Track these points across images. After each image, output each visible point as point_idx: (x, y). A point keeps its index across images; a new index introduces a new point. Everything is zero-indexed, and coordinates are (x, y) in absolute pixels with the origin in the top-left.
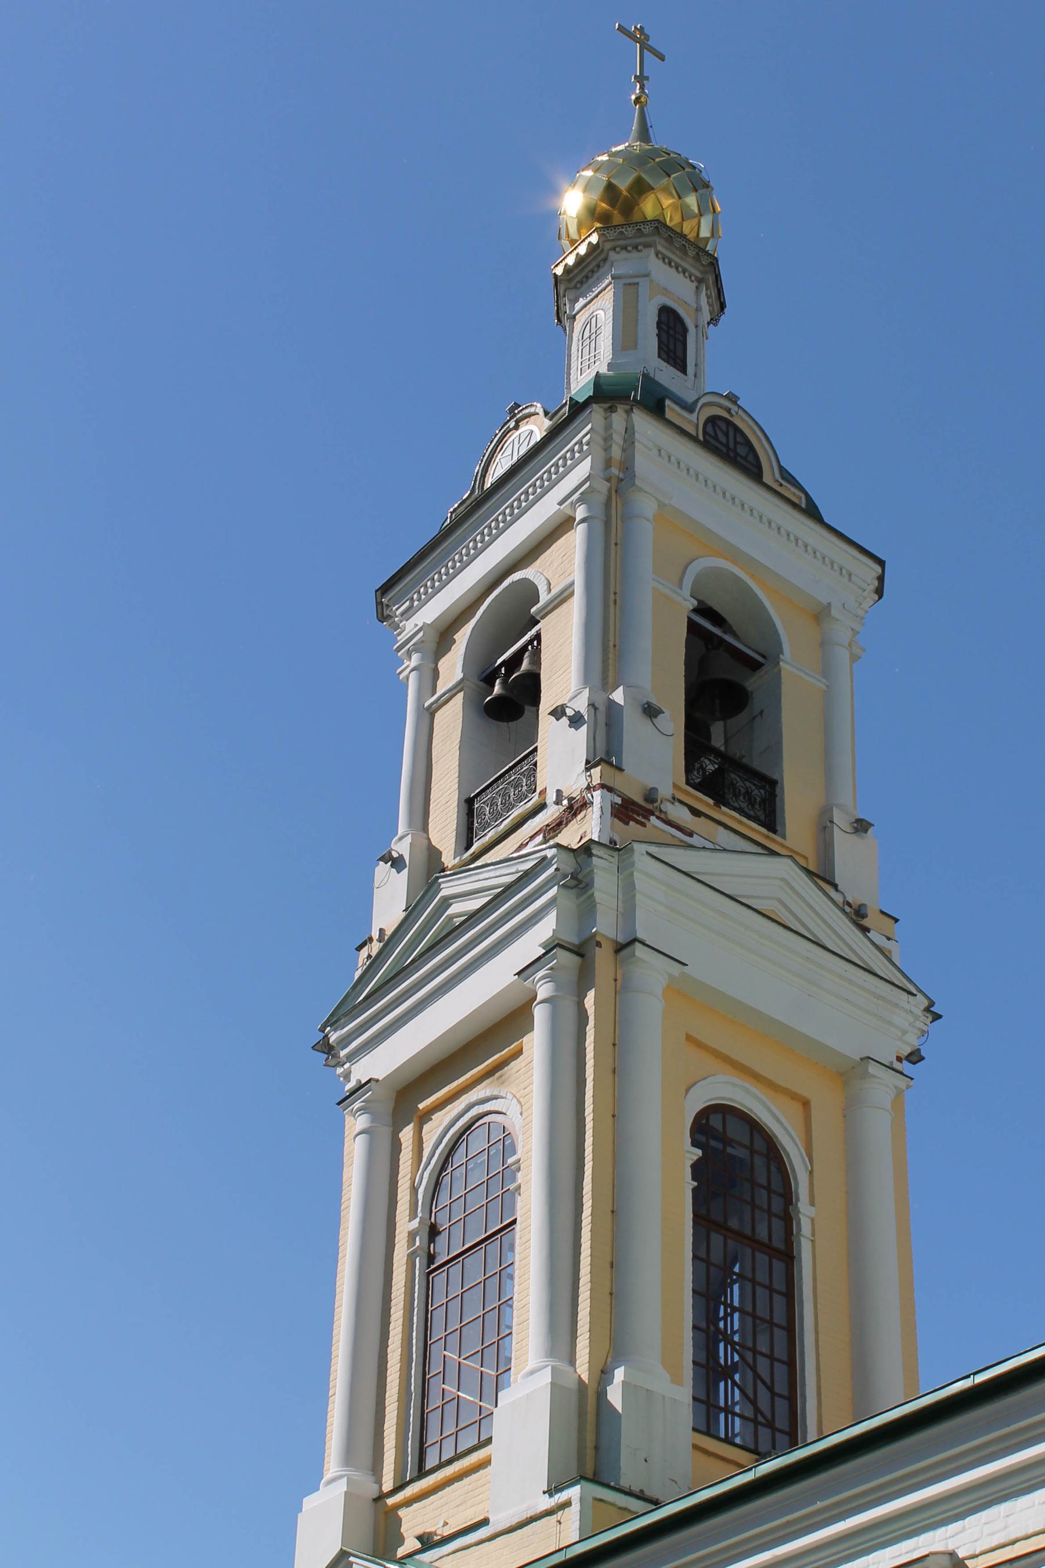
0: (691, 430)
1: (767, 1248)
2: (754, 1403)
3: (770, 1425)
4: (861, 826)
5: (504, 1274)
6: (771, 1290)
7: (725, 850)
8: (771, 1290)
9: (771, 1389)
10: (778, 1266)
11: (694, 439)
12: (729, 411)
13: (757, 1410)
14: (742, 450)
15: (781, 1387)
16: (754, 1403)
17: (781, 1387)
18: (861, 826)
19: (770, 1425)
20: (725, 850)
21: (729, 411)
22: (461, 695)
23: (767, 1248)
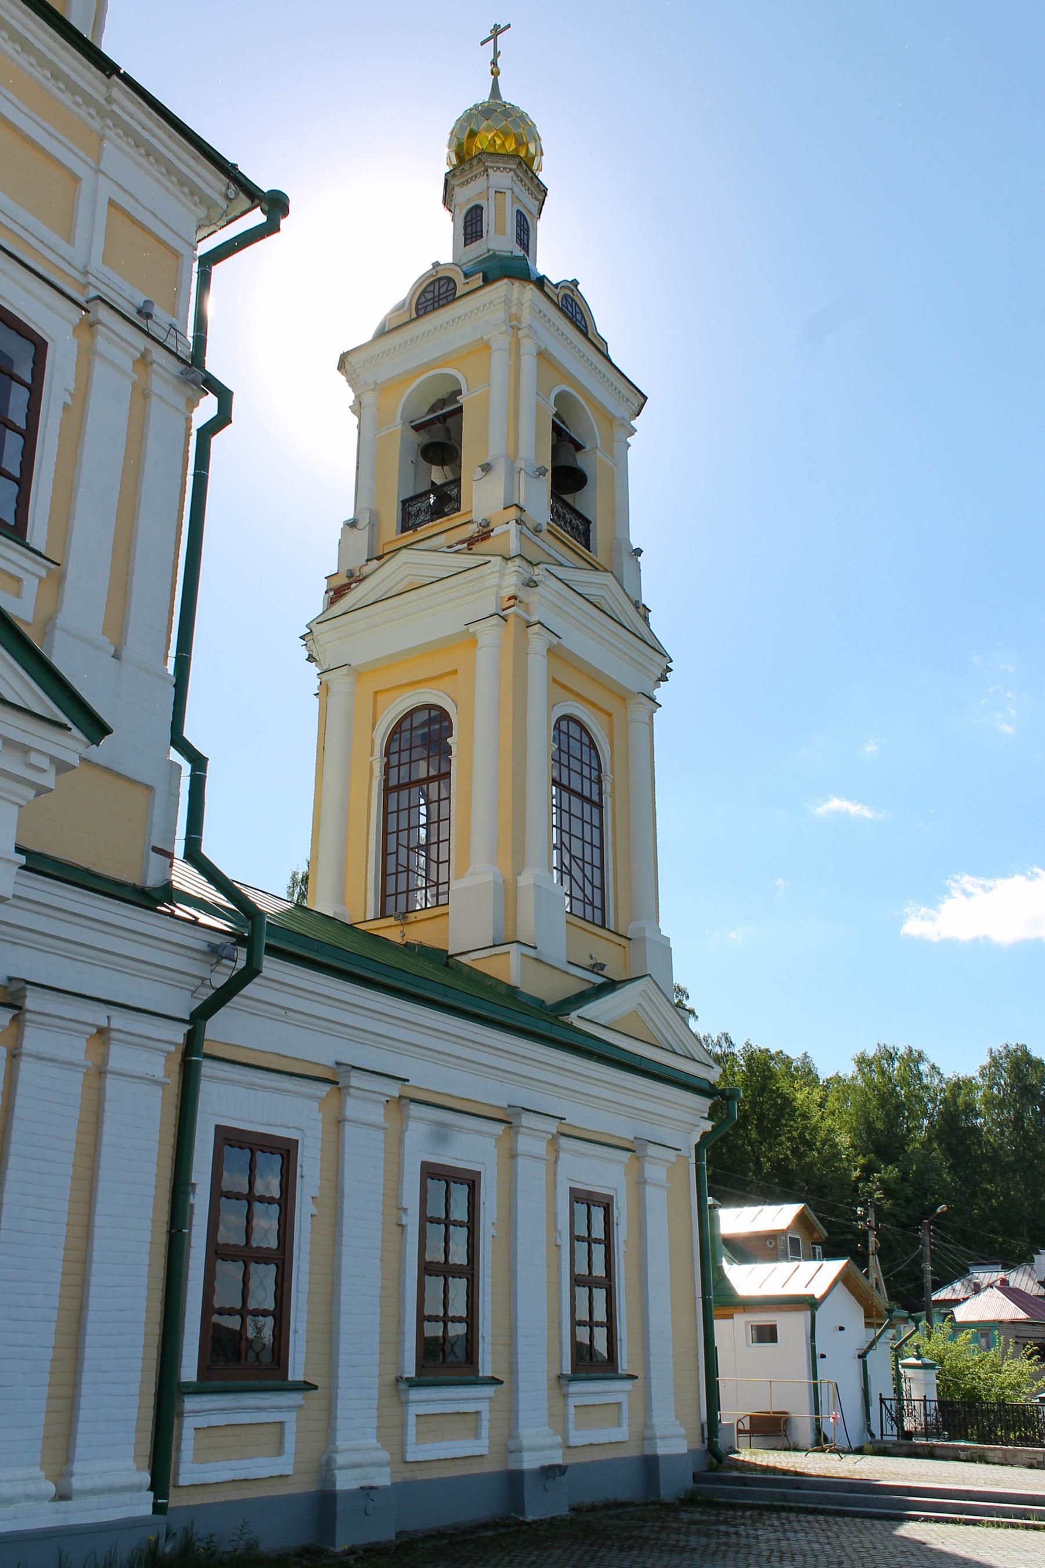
0: (555, 299)
1: (589, 800)
2: (583, 891)
3: (592, 904)
4: (823, 1356)
5: (581, 543)
6: (592, 825)
7: (694, 1060)
8: (592, 825)
9: (592, 884)
10: (595, 811)
11: (556, 305)
12: (573, 291)
13: (585, 895)
14: (579, 317)
15: (597, 882)
16: (583, 891)
17: (597, 903)
18: (823, 1356)
19: (592, 904)
20: (694, 1060)
21: (573, 291)
22: (564, 496)
23: (589, 800)
